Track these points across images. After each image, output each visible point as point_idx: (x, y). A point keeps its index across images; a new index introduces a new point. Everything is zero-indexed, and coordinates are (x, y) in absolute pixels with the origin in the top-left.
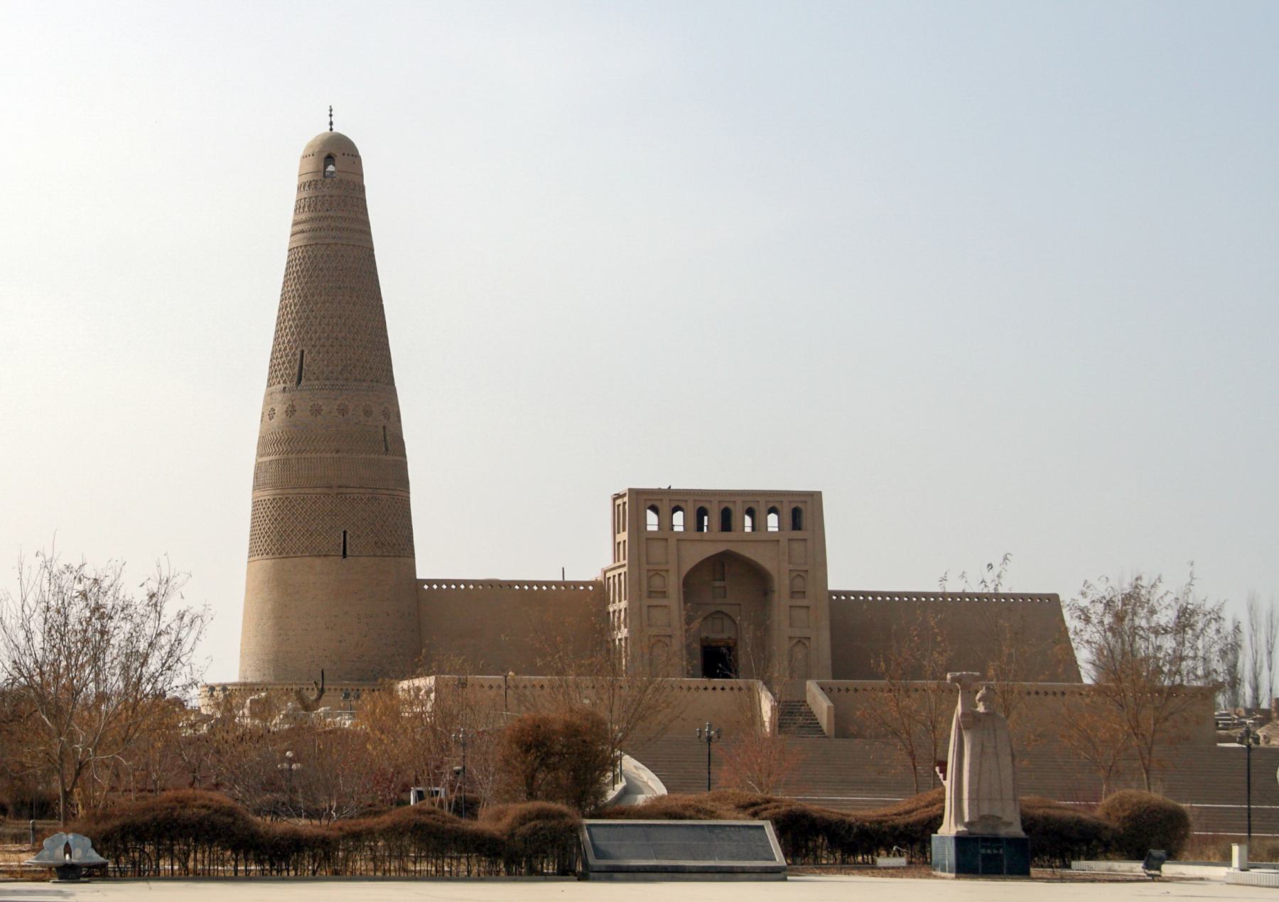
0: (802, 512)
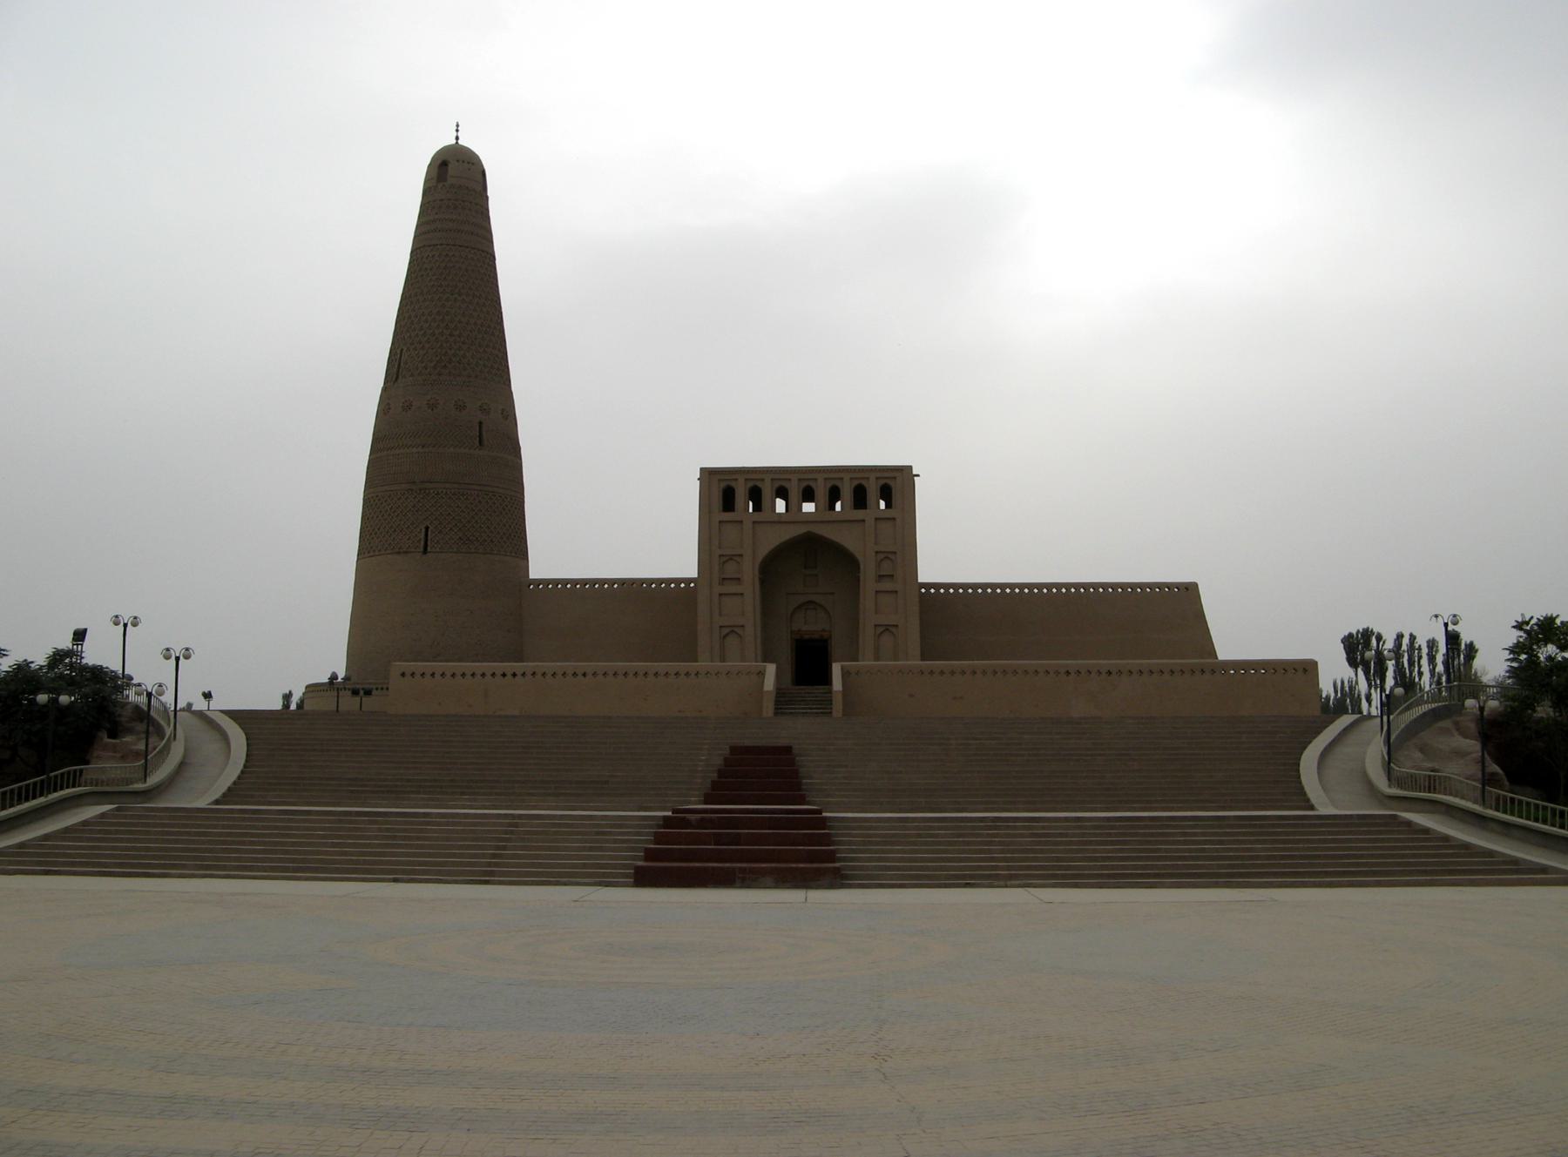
0: (888, 490)
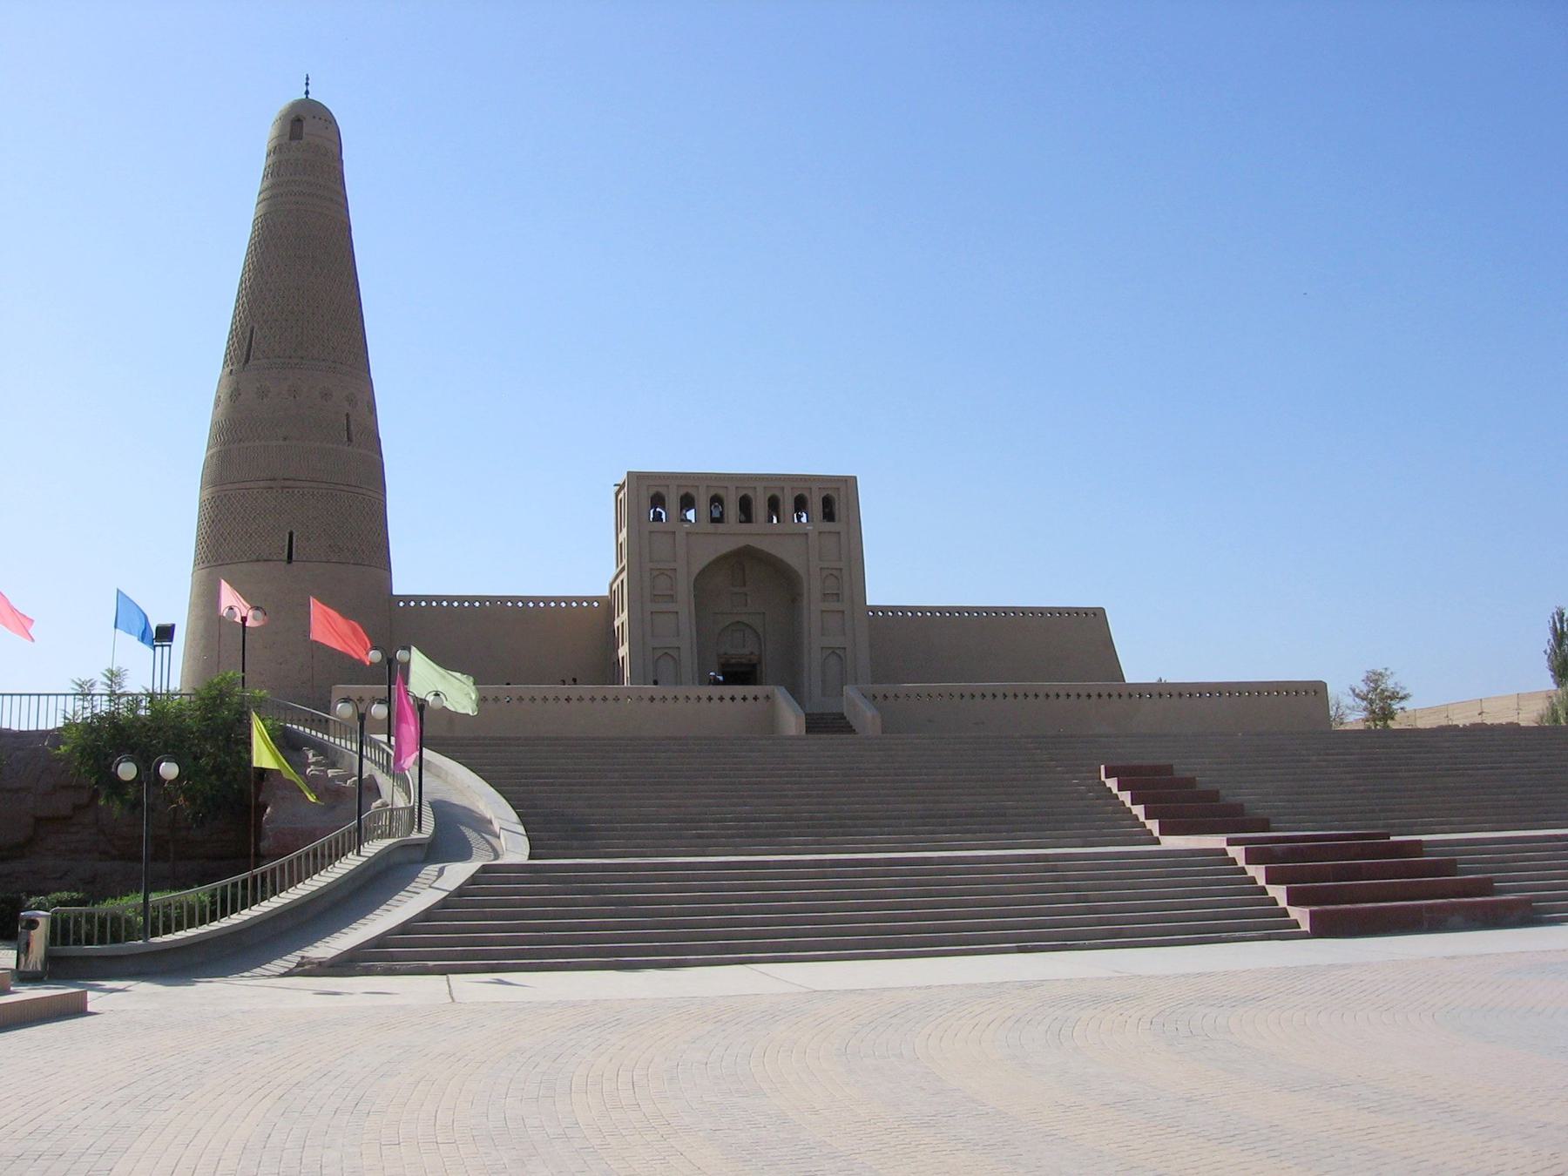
0: (831, 502)
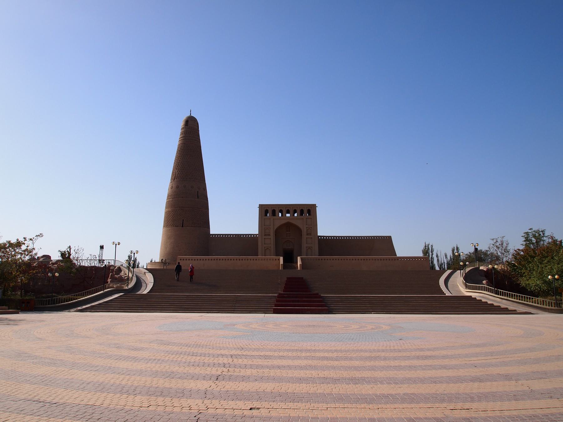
0: (308, 211)
